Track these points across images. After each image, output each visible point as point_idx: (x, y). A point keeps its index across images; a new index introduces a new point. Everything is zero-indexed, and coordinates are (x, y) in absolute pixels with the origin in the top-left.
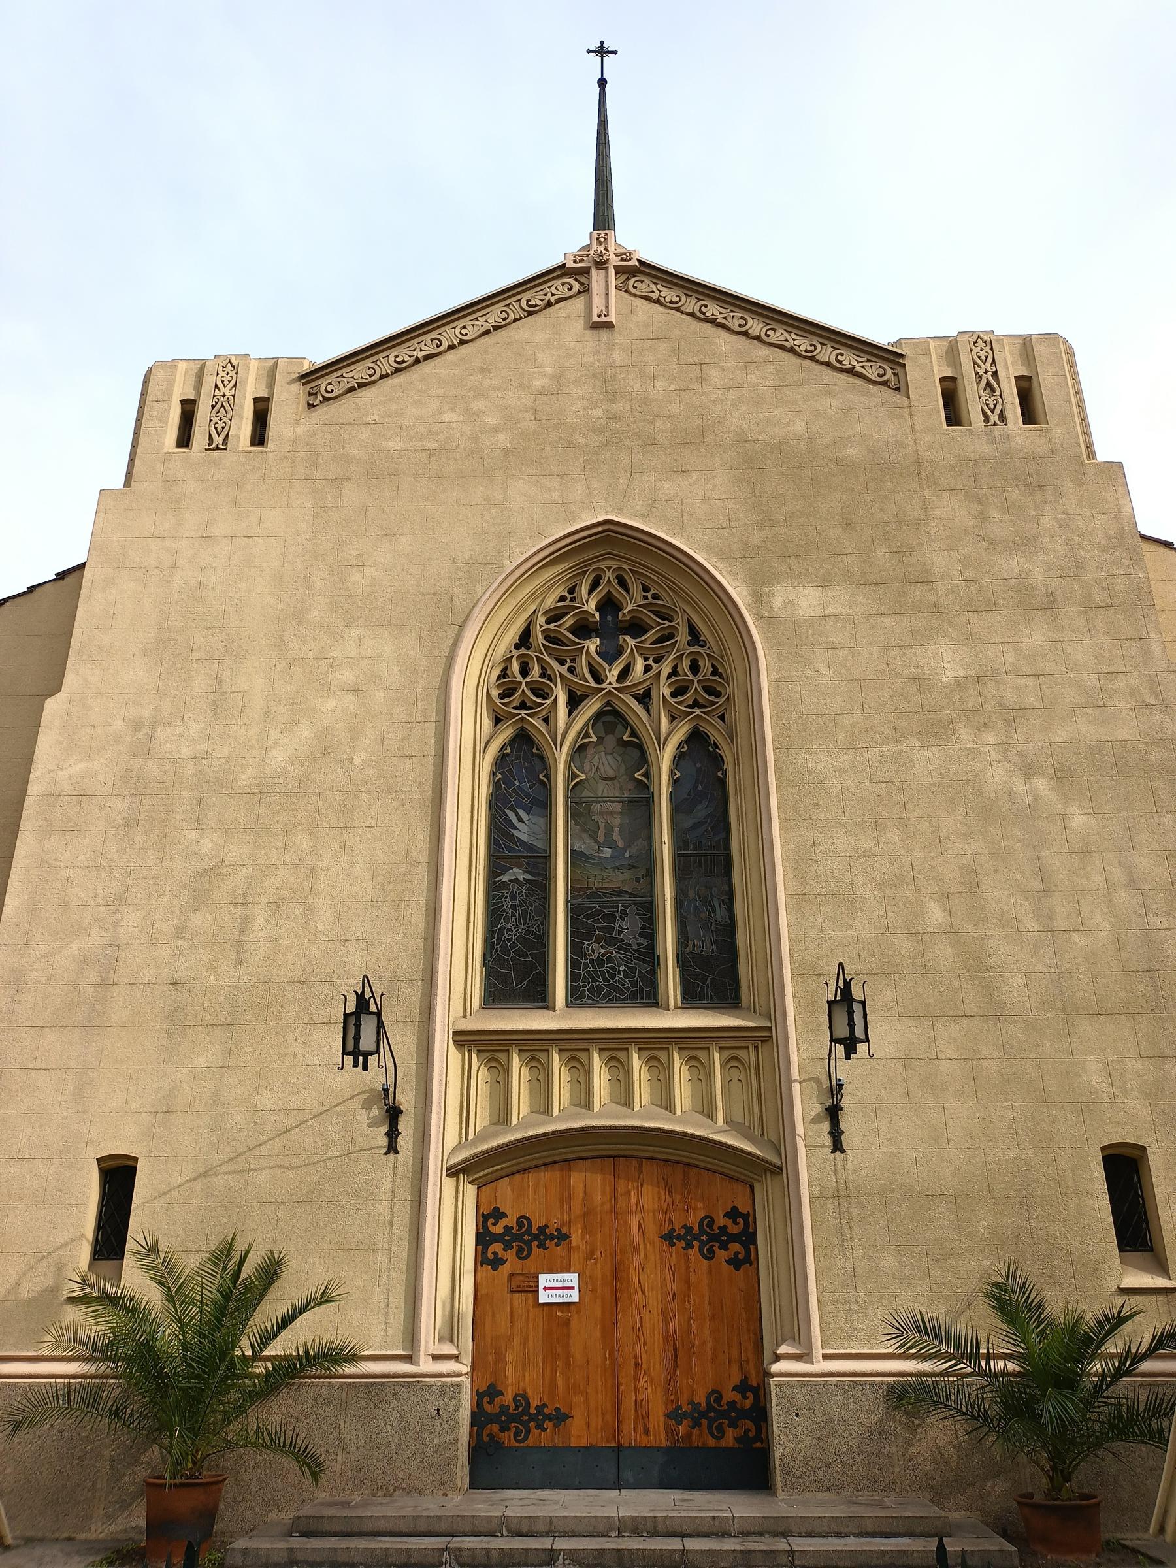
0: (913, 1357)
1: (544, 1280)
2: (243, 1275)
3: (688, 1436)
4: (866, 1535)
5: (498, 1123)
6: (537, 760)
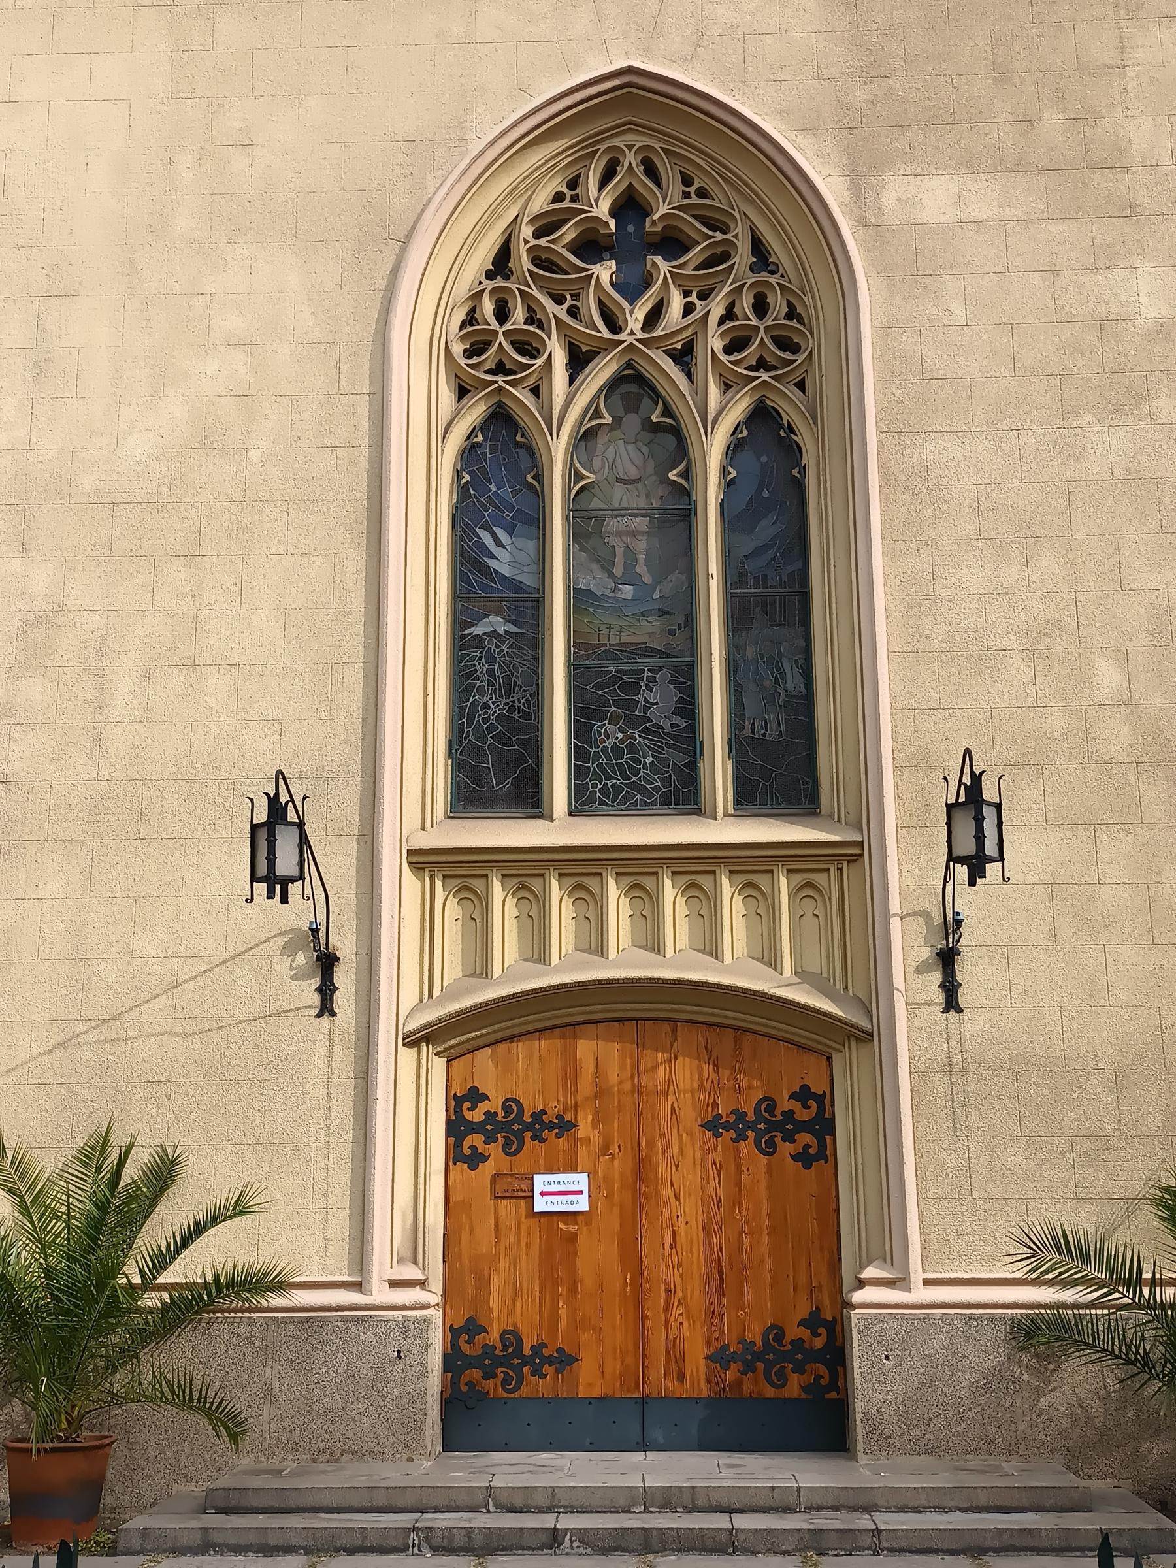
0: (1051, 1283)
1: (541, 1182)
2: (126, 1178)
3: (737, 1384)
4: (977, 1509)
5: (474, 975)
6: (522, 452)
